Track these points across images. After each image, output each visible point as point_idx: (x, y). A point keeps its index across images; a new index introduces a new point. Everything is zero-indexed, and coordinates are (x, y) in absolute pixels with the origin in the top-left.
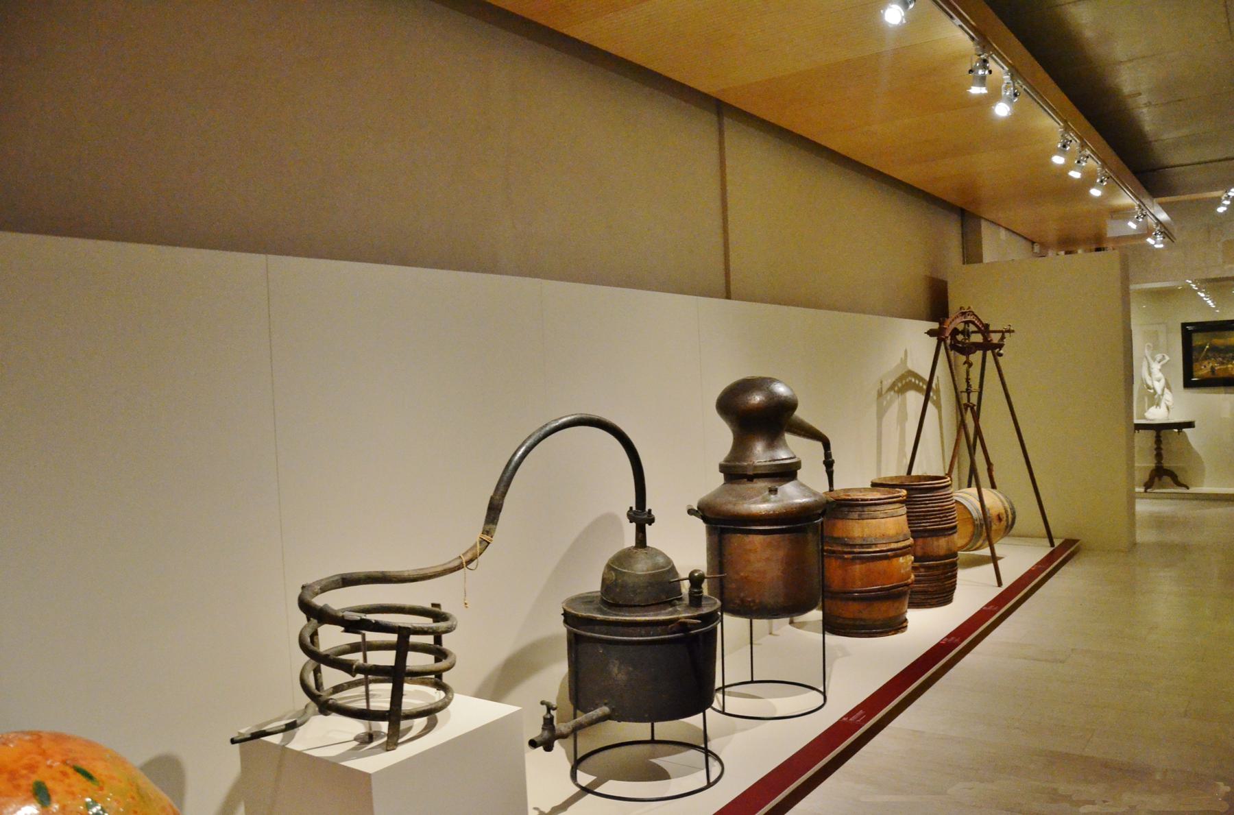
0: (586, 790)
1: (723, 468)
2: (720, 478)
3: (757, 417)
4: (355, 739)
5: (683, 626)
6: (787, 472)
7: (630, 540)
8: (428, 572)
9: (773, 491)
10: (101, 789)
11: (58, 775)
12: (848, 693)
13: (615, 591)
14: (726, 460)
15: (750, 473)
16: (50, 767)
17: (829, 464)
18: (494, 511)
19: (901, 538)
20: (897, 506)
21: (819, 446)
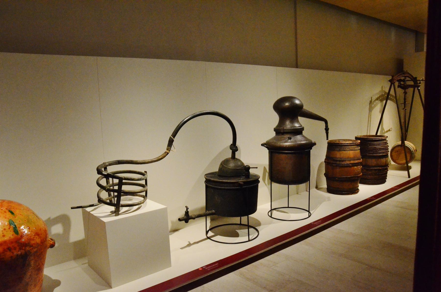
0: (208, 238)
1: (275, 130)
2: (274, 134)
3: (288, 110)
4: (111, 212)
5: (239, 185)
6: (299, 131)
7: (229, 155)
8: (146, 161)
9: (290, 138)
10: (15, 217)
11: (3, 212)
12: (319, 213)
13: (224, 172)
14: (277, 126)
15: (282, 131)
16: (2, 210)
17: (327, 129)
18: (171, 142)
19: (356, 159)
20: (355, 146)
21: (323, 123)
